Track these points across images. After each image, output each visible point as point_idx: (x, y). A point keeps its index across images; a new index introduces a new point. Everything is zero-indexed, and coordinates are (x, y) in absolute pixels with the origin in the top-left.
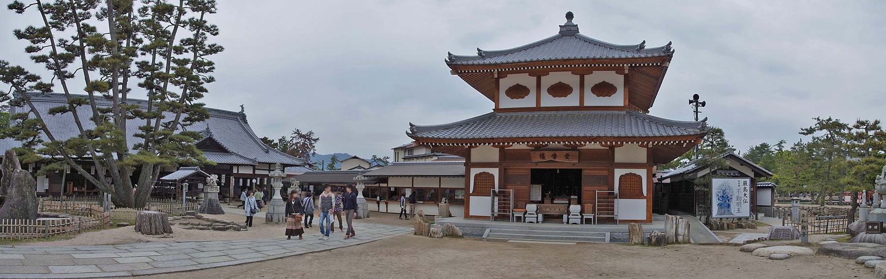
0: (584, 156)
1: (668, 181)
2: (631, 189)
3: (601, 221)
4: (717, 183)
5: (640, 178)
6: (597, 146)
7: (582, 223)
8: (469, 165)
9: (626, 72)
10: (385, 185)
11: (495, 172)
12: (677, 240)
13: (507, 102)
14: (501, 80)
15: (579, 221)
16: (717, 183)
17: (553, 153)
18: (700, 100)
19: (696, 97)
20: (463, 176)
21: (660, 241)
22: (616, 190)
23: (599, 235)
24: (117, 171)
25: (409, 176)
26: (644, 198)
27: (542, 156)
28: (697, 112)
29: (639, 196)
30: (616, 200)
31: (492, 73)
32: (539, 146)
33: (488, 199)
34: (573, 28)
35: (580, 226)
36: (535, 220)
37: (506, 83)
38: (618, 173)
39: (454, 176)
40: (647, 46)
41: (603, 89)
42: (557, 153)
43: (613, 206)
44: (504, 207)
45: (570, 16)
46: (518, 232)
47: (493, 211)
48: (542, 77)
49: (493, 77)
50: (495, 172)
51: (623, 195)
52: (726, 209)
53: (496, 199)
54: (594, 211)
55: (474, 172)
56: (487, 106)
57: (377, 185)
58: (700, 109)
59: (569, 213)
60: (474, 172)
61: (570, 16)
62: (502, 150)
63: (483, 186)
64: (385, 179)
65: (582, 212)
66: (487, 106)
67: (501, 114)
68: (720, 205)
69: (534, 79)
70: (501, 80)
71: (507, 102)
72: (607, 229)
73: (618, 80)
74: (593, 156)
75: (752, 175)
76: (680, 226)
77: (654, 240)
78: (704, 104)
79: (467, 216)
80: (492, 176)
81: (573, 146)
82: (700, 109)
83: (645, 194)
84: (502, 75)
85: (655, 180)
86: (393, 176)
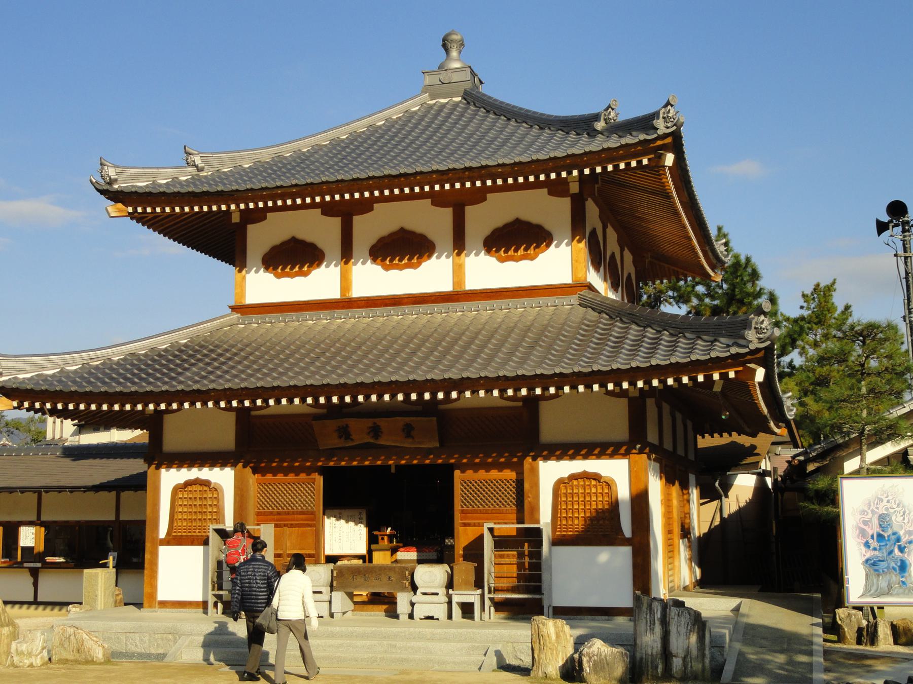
14: (250, 227)
15: (440, 611)
17: (369, 422)
19: (897, 209)
26: (625, 542)
27: (344, 433)
39: (74, 489)
42: (383, 422)
50: (223, 478)
51: (174, 539)
52: (895, 578)
54: (479, 583)
65: (450, 585)
68: (872, 564)
69: (447, 214)
70: (250, 227)
86: (60, 489)
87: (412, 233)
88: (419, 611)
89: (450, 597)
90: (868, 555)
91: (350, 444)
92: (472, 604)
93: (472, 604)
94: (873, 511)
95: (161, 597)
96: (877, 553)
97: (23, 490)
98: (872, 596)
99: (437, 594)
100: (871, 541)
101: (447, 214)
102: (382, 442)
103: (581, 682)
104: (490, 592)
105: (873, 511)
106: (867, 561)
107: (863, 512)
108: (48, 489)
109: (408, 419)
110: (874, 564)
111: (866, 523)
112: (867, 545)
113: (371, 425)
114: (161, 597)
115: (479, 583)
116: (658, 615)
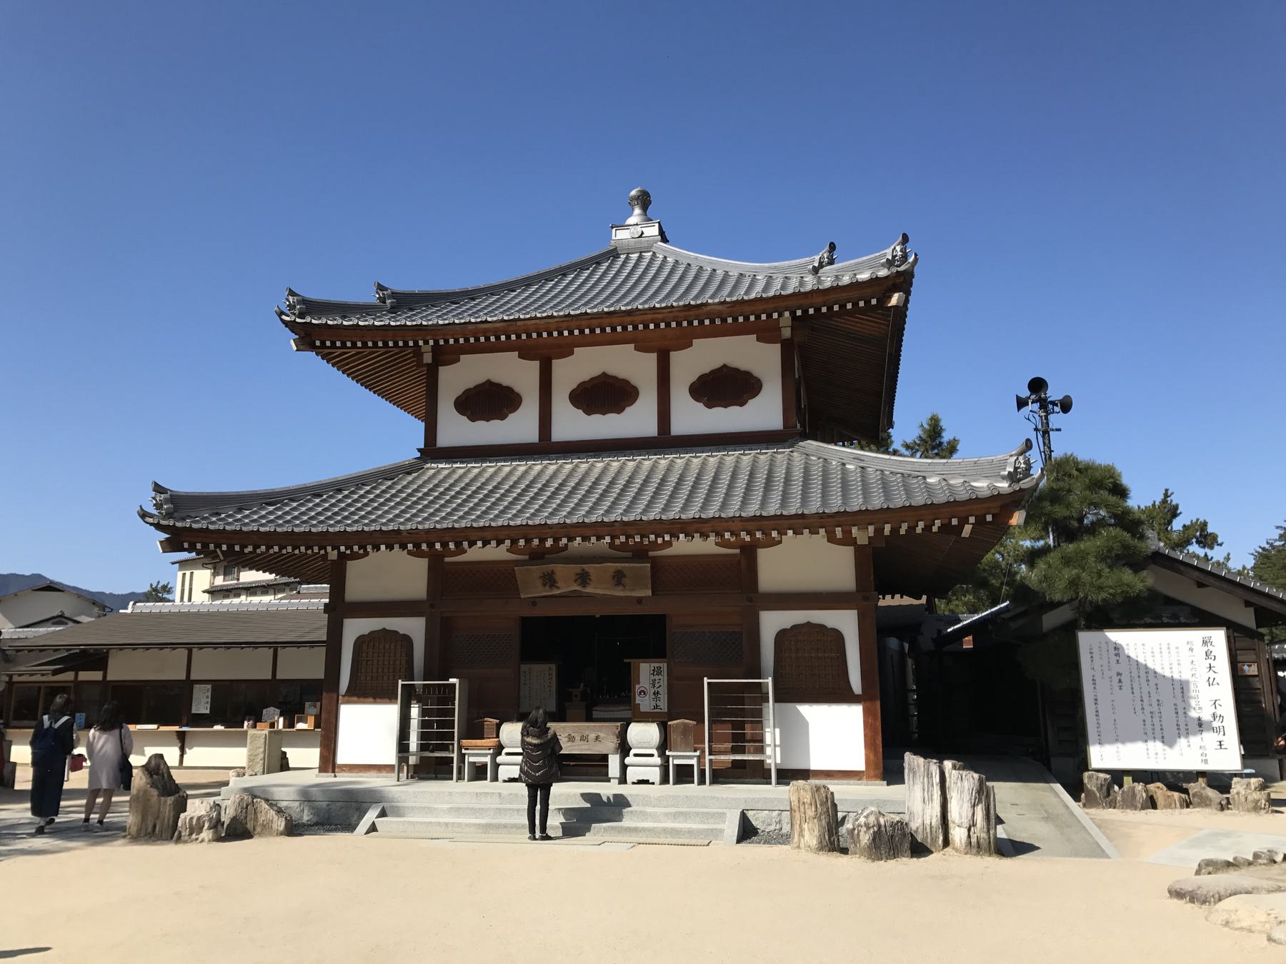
0: (669, 576)
6: (705, 546)
7: (665, 780)
9: (787, 333)
10: (96, 676)
11: (414, 627)
13: (456, 429)
15: (654, 774)
17: (577, 568)
18: (1054, 393)
19: (1037, 385)
21: (898, 842)
23: (706, 817)
24: (196, 587)
25: (174, 646)
27: (549, 580)
31: (417, 351)
32: (543, 546)
33: (391, 712)
35: (657, 790)
37: (458, 378)
38: (772, 623)
41: (725, 387)
42: (589, 568)
44: (436, 736)
47: (403, 747)
48: (555, 363)
49: (420, 364)
50: (414, 627)
53: (415, 711)
55: (354, 628)
57: (69, 676)
59: (624, 749)
60: (354, 628)
62: (436, 563)
64: (95, 657)
65: (663, 747)
69: (532, 369)
73: (763, 359)
74: (697, 574)
75: (1247, 618)
79: (328, 762)
81: (634, 543)
82: (1056, 419)
84: (446, 355)
88: (632, 774)
89: (666, 759)
91: (556, 592)
93: (485, 765)
95: (209, 686)
99: (652, 755)
101: (652, 358)
102: (589, 590)
103: (567, 809)
108: (202, 645)
109: (619, 565)
113: (579, 571)
114: (209, 686)
116: (936, 779)
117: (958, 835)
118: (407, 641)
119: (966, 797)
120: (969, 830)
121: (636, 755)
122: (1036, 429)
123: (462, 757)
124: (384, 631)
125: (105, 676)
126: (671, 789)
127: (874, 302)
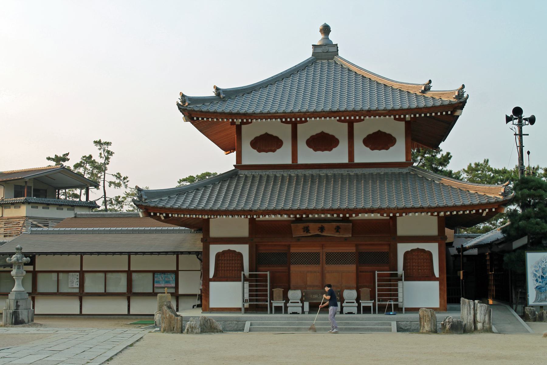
1: (475, 252)
2: (418, 269)
3: (382, 309)
4: (533, 259)
5: (430, 254)
8: (207, 241)
11: (244, 249)
12: (476, 328)
13: (252, 157)
15: (355, 310)
16: (533, 259)
17: (320, 225)
18: (526, 115)
19: (518, 111)
20: (197, 253)
21: (458, 328)
22: (400, 270)
25: (76, 253)
26: (435, 279)
27: (307, 230)
28: (521, 135)
29: (430, 277)
30: (400, 284)
33: (239, 284)
34: (332, 49)
36: (299, 310)
38: (403, 248)
40: (434, 87)
42: (325, 225)
43: (397, 290)
45: (326, 30)
46: (285, 324)
51: (409, 277)
53: (247, 284)
56: (225, 162)
58: (526, 129)
60: (215, 249)
61: (326, 30)
62: (252, 222)
63: (228, 268)
65: (358, 300)
66: (225, 162)
67: (246, 172)
68: (538, 289)
71: (252, 157)
72: (392, 319)
76: (478, 312)
77: (448, 326)
78: (532, 120)
80: (240, 255)
83: (437, 274)
85: (453, 251)
86: (91, 253)
87: (327, 135)
89: (359, 305)
90: (537, 285)
92: (371, 306)
94: (540, 267)
96: (541, 284)
97: (121, 253)
98: (539, 302)
100: (538, 279)
104: (379, 301)
105: (540, 267)
106: (537, 287)
107: (535, 267)
109: (338, 224)
110: (539, 289)
111: (536, 271)
112: (537, 280)
113: (320, 226)
114: (212, 305)
115: (372, 298)
116: (472, 307)
117: (479, 326)
118: (240, 256)
119: (483, 312)
120: (483, 324)
121: (347, 303)
122: (516, 135)
123: (271, 304)
124: (229, 251)
125: (34, 268)
126: (362, 316)
127: (449, 113)
